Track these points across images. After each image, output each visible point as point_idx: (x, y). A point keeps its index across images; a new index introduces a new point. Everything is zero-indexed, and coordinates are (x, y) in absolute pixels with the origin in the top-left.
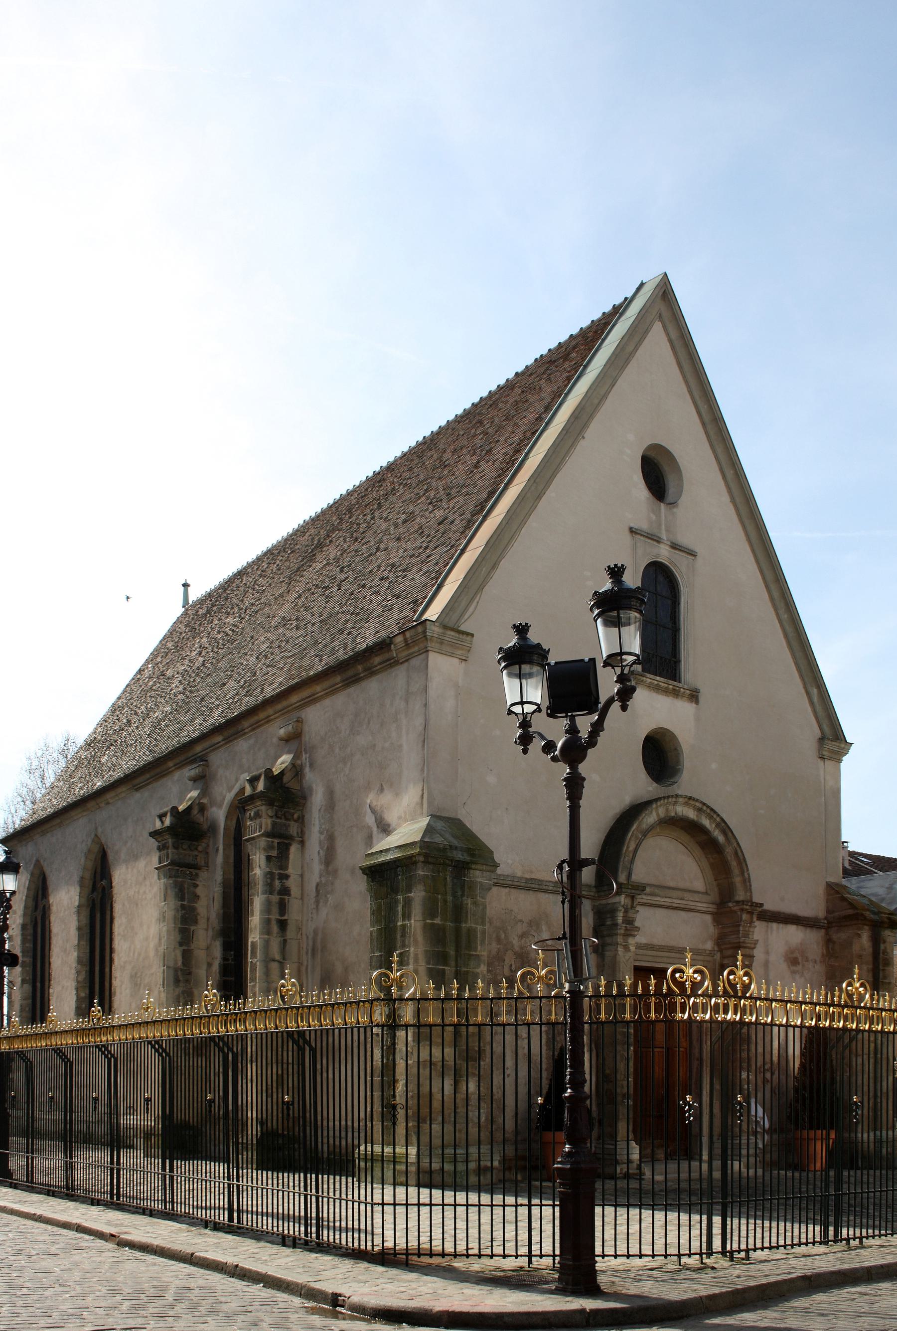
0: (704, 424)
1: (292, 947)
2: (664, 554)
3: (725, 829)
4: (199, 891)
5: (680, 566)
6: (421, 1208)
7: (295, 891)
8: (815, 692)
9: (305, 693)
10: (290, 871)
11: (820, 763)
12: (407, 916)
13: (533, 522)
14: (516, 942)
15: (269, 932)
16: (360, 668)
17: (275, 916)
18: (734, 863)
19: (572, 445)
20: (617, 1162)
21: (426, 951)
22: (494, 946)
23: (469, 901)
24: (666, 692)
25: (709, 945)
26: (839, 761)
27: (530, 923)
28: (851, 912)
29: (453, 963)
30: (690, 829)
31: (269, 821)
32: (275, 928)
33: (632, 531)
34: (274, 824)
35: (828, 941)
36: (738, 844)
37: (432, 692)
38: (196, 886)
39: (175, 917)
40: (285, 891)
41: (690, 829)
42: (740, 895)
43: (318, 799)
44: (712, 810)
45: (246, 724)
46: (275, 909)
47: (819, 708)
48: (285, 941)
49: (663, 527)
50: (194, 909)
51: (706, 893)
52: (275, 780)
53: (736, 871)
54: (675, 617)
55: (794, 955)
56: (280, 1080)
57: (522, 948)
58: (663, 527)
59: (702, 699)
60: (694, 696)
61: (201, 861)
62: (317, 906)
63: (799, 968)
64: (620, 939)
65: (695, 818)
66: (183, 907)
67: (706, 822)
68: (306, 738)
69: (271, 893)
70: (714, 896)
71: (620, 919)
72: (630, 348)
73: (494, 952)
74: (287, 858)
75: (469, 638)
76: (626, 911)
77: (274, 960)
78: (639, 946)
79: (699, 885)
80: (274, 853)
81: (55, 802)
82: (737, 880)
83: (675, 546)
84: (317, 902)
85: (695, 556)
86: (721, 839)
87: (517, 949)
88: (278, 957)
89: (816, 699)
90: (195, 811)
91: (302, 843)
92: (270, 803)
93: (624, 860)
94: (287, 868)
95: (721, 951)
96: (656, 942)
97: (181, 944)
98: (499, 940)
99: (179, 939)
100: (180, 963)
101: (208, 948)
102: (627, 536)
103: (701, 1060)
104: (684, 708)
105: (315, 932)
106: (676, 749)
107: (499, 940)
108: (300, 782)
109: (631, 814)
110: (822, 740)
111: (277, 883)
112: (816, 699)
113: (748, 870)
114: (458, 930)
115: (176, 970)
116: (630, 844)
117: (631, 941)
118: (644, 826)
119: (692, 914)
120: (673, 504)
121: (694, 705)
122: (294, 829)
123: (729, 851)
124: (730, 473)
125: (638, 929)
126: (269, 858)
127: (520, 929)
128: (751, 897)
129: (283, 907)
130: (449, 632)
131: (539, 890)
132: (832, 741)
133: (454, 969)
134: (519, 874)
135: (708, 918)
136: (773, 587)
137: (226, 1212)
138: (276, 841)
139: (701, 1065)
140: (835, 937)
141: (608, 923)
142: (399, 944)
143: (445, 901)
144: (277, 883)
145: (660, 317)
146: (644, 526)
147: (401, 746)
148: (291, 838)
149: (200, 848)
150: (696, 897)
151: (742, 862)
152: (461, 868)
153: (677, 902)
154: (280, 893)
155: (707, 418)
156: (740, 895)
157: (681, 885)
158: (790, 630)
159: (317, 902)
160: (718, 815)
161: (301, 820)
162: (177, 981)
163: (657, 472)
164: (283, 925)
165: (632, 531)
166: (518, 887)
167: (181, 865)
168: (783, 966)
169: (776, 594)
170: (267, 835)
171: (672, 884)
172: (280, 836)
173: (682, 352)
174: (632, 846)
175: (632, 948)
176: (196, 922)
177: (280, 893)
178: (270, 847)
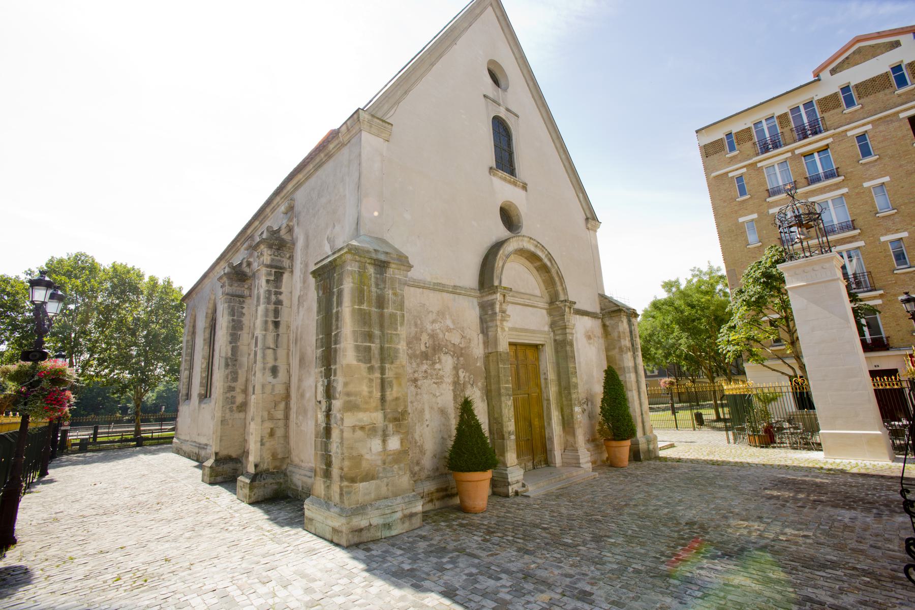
1: (283, 339)
3: (551, 259)
4: (244, 311)
5: (511, 121)
7: (286, 302)
8: (581, 195)
9: (294, 181)
10: (283, 289)
12: (339, 303)
13: (429, 77)
14: (429, 327)
15: (266, 330)
16: (322, 155)
17: (271, 318)
18: (557, 279)
19: (448, 47)
20: (509, 484)
21: (354, 332)
22: (413, 330)
23: (390, 292)
24: (510, 182)
25: (547, 328)
26: (596, 231)
27: (438, 313)
28: (616, 308)
29: (377, 341)
30: (532, 257)
31: (269, 258)
32: (271, 326)
33: (485, 96)
34: (273, 260)
35: (604, 326)
37: (364, 156)
38: (243, 308)
39: (228, 327)
40: (279, 303)
41: (532, 257)
42: (562, 298)
43: (300, 244)
45: (268, 210)
46: (271, 314)
47: (584, 204)
48: (278, 335)
50: (240, 322)
52: (274, 233)
53: (558, 284)
54: (511, 154)
56: (272, 434)
57: (433, 331)
60: (524, 187)
61: (246, 292)
63: (591, 341)
64: (498, 323)
66: (233, 320)
68: (296, 209)
69: (269, 303)
70: (547, 298)
71: (497, 310)
72: (477, 11)
73: (413, 334)
74: (281, 281)
75: (389, 126)
76: (501, 304)
77: (269, 348)
78: (511, 329)
79: (537, 292)
80: (272, 278)
82: (559, 288)
83: (508, 110)
84: (298, 308)
86: (549, 264)
87: (430, 331)
88: (272, 346)
90: (244, 265)
91: (292, 272)
92: (270, 247)
93: (497, 272)
94: (280, 288)
95: (554, 331)
96: (517, 326)
97: (231, 343)
98: (416, 325)
99: (229, 339)
100: (229, 354)
101: (249, 345)
103: (548, 400)
104: (519, 192)
105: (297, 328)
107: (416, 325)
108: (292, 236)
109: (497, 247)
110: (587, 219)
111: (273, 298)
114: (381, 316)
115: (226, 359)
116: (499, 263)
117: (505, 323)
118: (506, 253)
119: (535, 309)
120: (505, 90)
122: (286, 263)
123: (553, 271)
124: (531, 84)
125: (509, 316)
126: (268, 281)
127: (432, 317)
129: (277, 313)
130: (375, 120)
131: (443, 291)
132: (591, 219)
133: (378, 346)
134: (429, 279)
135: (544, 312)
136: (556, 141)
138: (273, 270)
139: (549, 404)
140: (607, 323)
141: (490, 312)
142: (334, 328)
143: (370, 291)
144: (273, 298)
145: (491, 5)
147: (345, 196)
148: (284, 268)
149: (246, 286)
150: (538, 299)
151: (561, 278)
152: (382, 266)
153: (527, 302)
154: (275, 303)
155: (517, 56)
156: (562, 298)
157: (528, 292)
158: (567, 164)
159: (298, 308)
161: (291, 258)
162: (227, 365)
164: (277, 324)
165: (485, 96)
166: (428, 288)
167: (232, 295)
168: (584, 340)
169: (558, 145)
170: (267, 266)
171: (522, 291)
172: (276, 267)
173: (503, 23)
174: (501, 265)
175: (507, 329)
176: (242, 329)
177: (275, 303)
178: (269, 274)
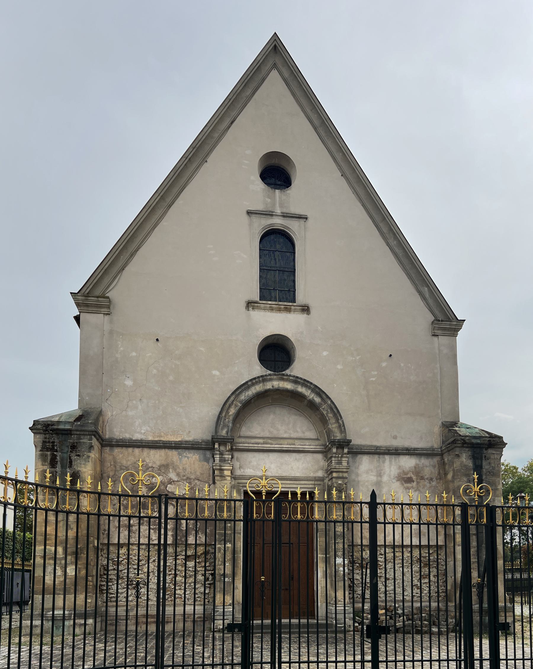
0: (315, 129)
2: (278, 222)
5: (294, 228)
6: (521, 657)
11: (435, 339)
33: (249, 213)
36: (332, 401)
44: (305, 380)
47: (430, 301)
49: (278, 205)
51: (318, 439)
55: (409, 476)
58: (278, 205)
59: (312, 311)
60: (306, 309)
62: (102, 475)
65: (292, 388)
67: (301, 389)
81: (163, 462)
85: (306, 218)
86: (317, 400)
89: (427, 295)
102: (246, 217)
106: (293, 348)
112: (427, 295)
113: (341, 418)
121: (305, 315)
124: (339, 157)
128: (345, 436)
137: (477, 655)
146: (260, 207)
153: (285, 446)
160: (311, 383)
163: (276, 173)
